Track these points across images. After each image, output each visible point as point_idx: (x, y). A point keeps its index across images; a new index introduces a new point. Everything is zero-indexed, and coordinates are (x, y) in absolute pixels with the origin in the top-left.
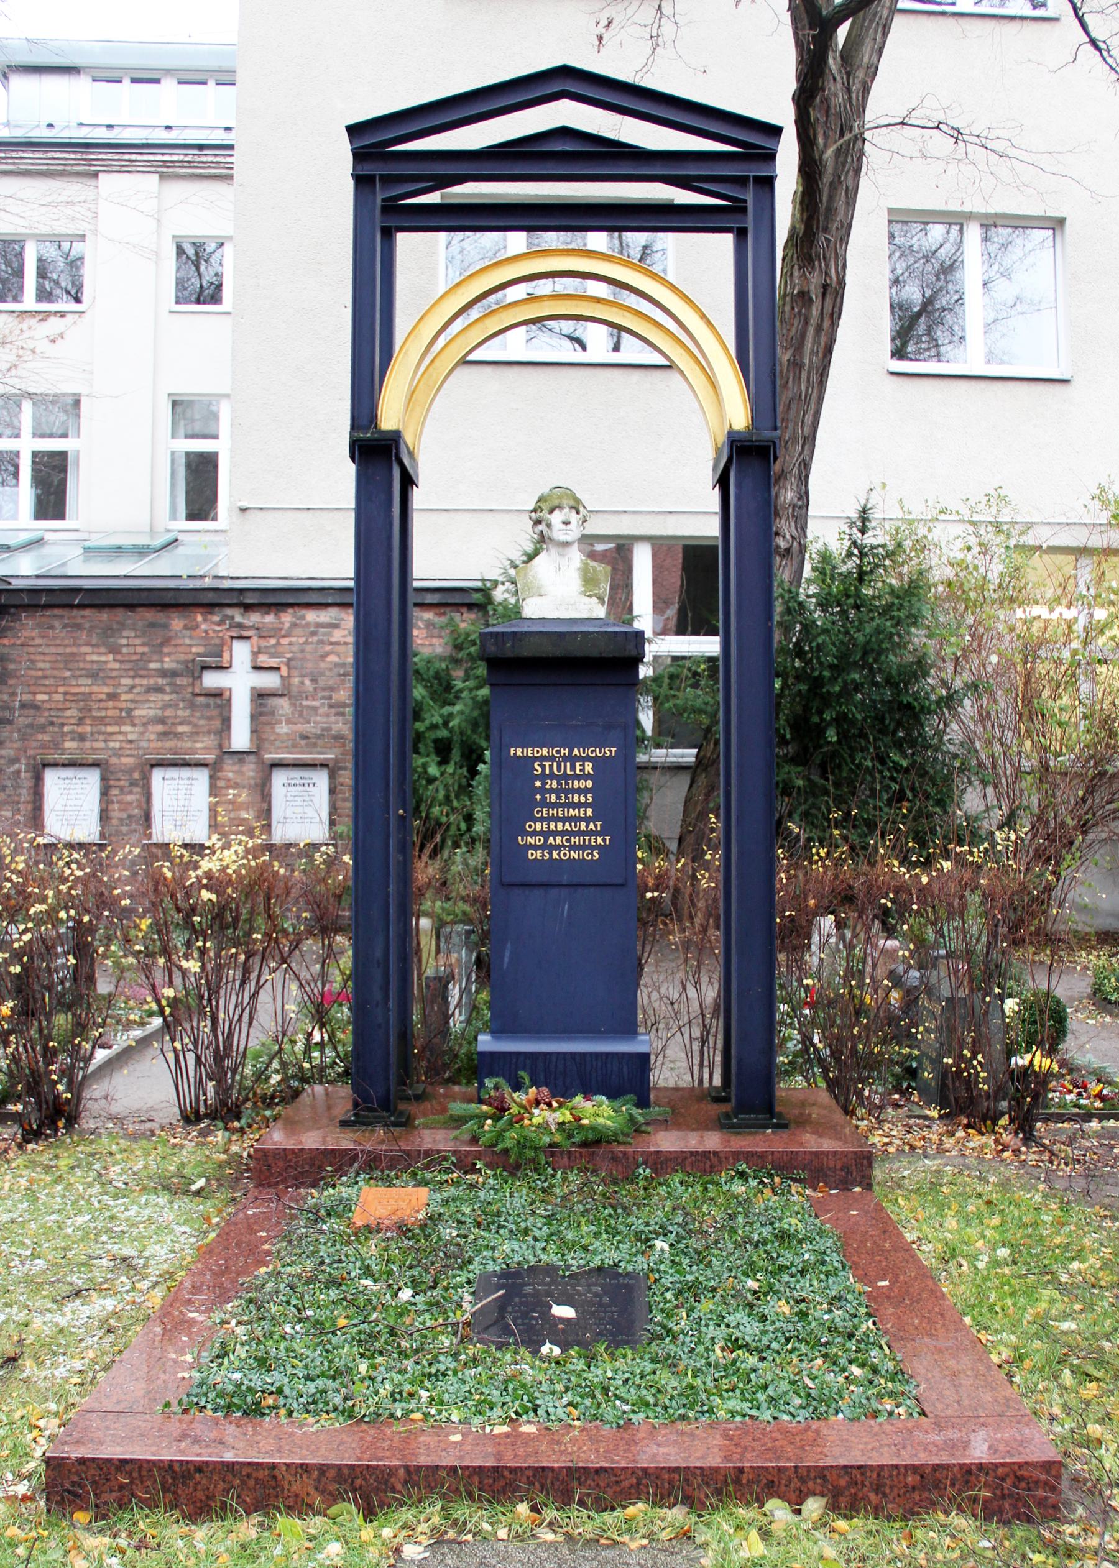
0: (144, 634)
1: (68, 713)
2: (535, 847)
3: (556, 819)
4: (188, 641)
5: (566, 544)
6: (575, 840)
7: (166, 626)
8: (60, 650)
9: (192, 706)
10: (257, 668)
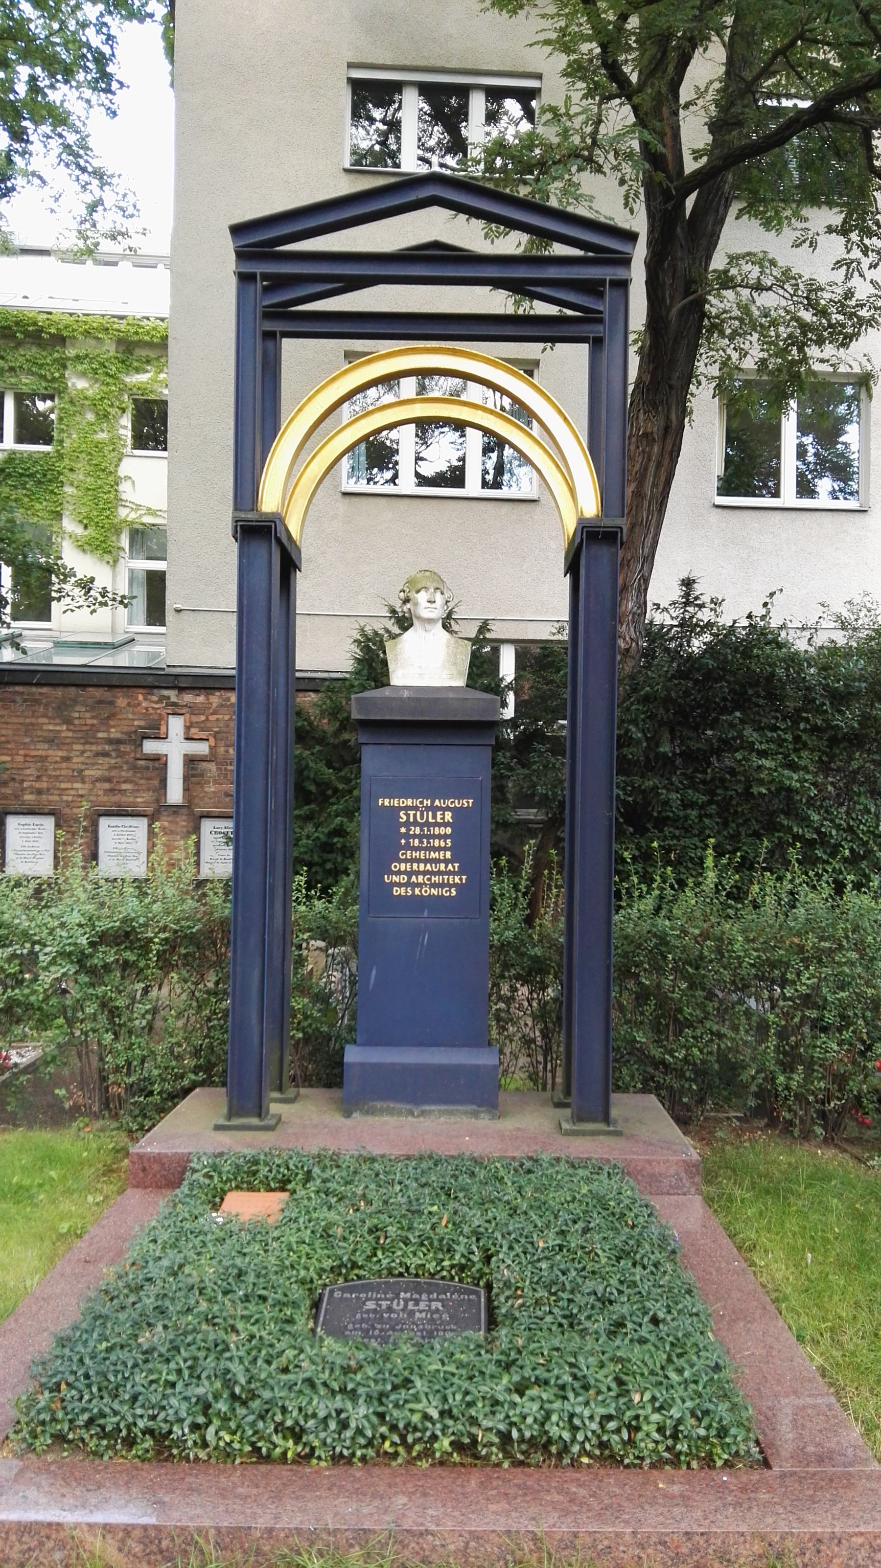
0: (93, 709)
1: (28, 772)
2: (400, 885)
3: (418, 861)
4: (130, 716)
5: (430, 621)
6: (435, 879)
7: (112, 703)
8: (21, 720)
9: (134, 768)
10: (188, 739)
